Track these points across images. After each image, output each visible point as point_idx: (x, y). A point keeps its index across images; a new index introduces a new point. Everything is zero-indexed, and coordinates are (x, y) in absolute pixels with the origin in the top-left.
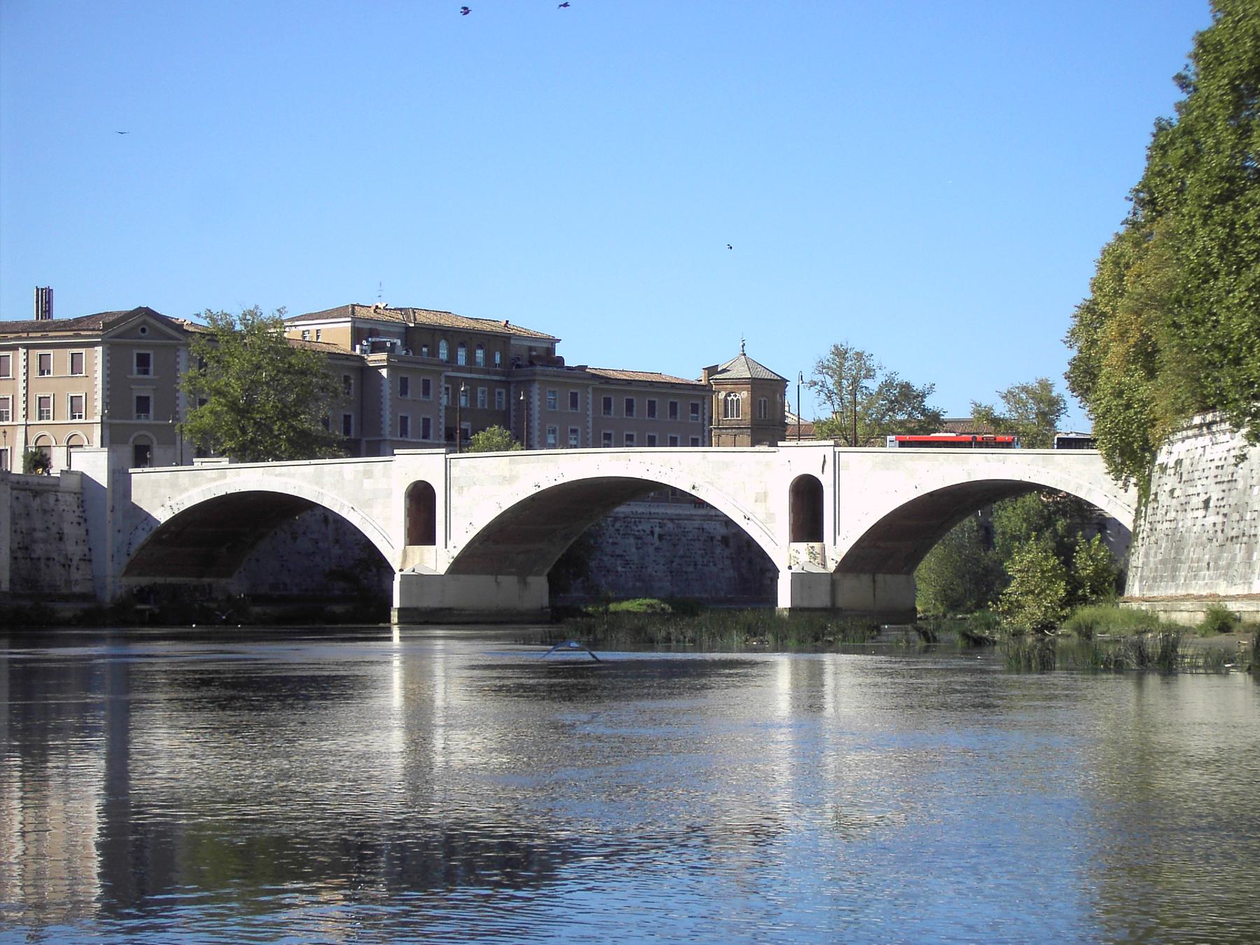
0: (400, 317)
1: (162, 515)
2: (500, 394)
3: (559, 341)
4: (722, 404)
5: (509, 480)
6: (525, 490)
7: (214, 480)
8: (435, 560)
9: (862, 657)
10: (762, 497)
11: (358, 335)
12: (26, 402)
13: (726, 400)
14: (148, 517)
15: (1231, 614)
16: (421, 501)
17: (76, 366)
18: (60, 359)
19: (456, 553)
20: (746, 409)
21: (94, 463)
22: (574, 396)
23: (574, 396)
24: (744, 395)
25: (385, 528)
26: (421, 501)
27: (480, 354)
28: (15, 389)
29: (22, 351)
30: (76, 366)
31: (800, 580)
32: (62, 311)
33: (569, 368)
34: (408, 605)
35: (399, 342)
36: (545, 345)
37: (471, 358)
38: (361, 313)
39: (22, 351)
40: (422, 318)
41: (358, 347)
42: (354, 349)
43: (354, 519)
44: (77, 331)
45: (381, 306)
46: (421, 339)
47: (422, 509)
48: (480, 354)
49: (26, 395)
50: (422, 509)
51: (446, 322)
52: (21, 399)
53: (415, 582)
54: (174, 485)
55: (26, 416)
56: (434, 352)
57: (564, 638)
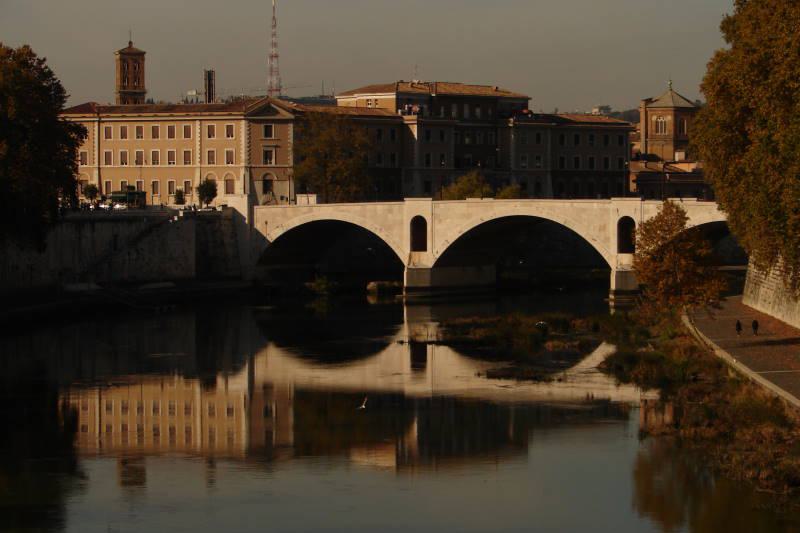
0: (426, 90)
1: (273, 234)
2: (491, 135)
3: (530, 99)
4: (654, 124)
5: (468, 216)
6: (466, 226)
7: (305, 213)
8: (428, 259)
9: (750, 305)
10: (603, 228)
11: (400, 103)
12: (201, 154)
13: (657, 122)
14: (264, 238)
15: (681, 321)
16: (419, 227)
17: (230, 133)
18: (220, 127)
19: (438, 256)
20: (670, 128)
21: (238, 202)
22: (538, 136)
23: (538, 136)
24: (669, 118)
25: (400, 243)
26: (419, 227)
27: (478, 111)
28: (194, 146)
29: (198, 123)
30: (230, 133)
31: (622, 275)
32: (224, 91)
33: (537, 117)
34: (411, 285)
35: (425, 106)
36: (522, 102)
37: (472, 113)
38: (403, 88)
39: (198, 123)
40: (442, 90)
41: (400, 111)
42: (397, 112)
43: (382, 235)
44: (232, 106)
45: (416, 81)
46: (438, 105)
47: (419, 231)
48: (478, 111)
49: (201, 150)
50: (419, 231)
51: (455, 91)
52: (198, 151)
53: (417, 272)
54: (285, 216)
55: (201, 162)
56: (448, 113)
57: (653, 259)
